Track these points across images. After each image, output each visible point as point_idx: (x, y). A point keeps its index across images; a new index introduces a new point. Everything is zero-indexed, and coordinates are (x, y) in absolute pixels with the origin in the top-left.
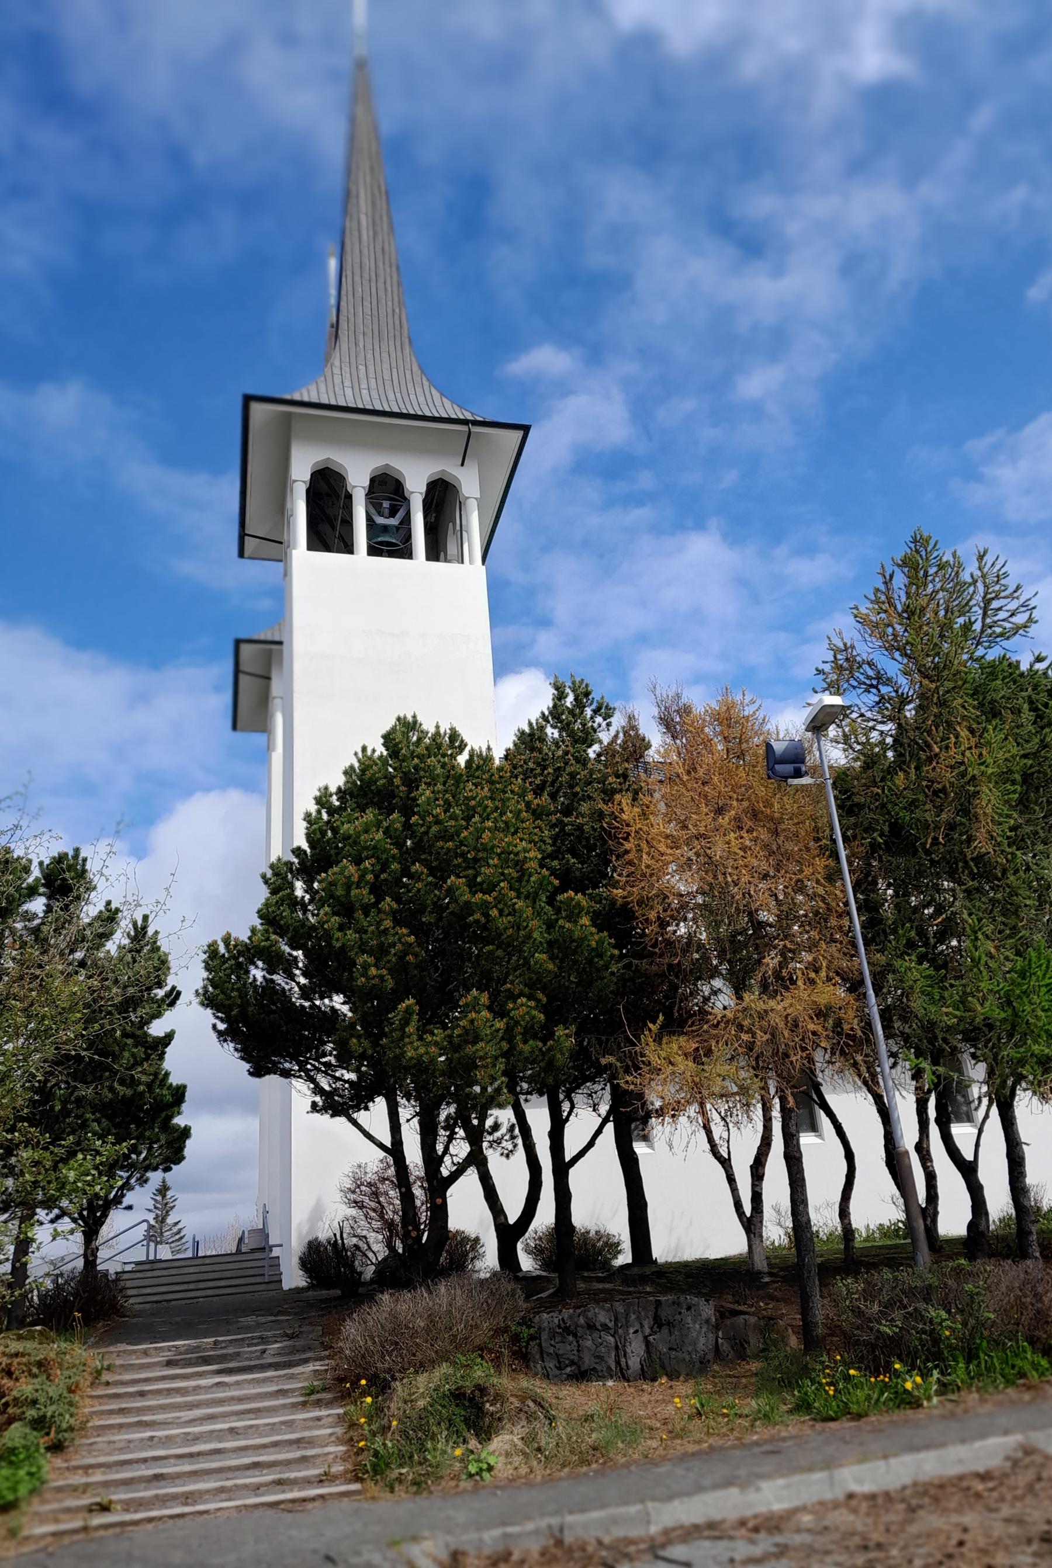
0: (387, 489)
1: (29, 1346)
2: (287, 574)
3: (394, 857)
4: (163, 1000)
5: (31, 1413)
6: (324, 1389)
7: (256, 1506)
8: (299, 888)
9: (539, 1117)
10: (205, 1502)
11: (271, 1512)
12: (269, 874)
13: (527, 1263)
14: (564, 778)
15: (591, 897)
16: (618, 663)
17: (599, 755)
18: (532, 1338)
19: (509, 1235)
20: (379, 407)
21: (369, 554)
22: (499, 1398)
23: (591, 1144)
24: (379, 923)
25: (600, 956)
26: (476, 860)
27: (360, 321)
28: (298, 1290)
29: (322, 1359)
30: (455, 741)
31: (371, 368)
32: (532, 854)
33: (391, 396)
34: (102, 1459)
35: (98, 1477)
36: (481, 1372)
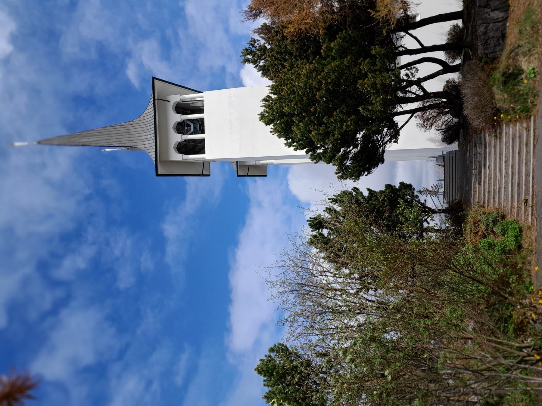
0: (181, 128)
1: (468, 227)
2: (214, 161)
3: (309, 119)
4: (356, 192)
5: (491, 225)
6: (496, 132)
7: (534, 152)
8: (320, 151)
9: (404, 60)
10: (530, 169)
11: (537, 147)
12: (315, 161)
13: (458, 62)
14: (278, 56)
15: (323, 43)
16: (235, 40)
17: (269, 44)
18: (487, 57)
19: (447, 69)
20: (154, 131)
21: (204, 133)
22: (508, 68)
23: (416, 38)
24: (333, 123)
25: (345, 37)
26: (310, 88)
27: (125, 139)
28: (459, 145)
29: (485, 134)
30: (267, 99)
31: (140, 135)
32: (308, 67)
33: (149, 127)
34: (510, 203)
35: (515, 204)
36: (497, 75)
